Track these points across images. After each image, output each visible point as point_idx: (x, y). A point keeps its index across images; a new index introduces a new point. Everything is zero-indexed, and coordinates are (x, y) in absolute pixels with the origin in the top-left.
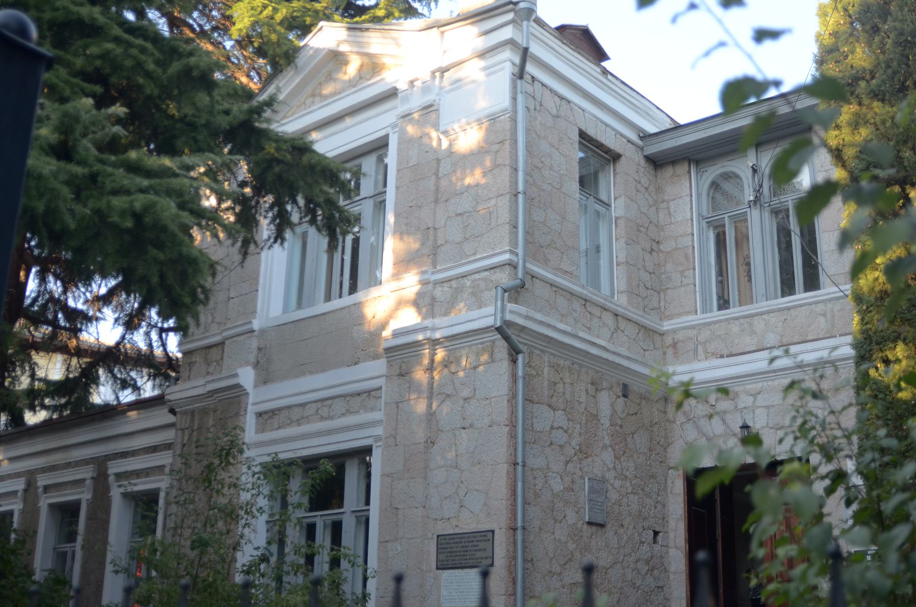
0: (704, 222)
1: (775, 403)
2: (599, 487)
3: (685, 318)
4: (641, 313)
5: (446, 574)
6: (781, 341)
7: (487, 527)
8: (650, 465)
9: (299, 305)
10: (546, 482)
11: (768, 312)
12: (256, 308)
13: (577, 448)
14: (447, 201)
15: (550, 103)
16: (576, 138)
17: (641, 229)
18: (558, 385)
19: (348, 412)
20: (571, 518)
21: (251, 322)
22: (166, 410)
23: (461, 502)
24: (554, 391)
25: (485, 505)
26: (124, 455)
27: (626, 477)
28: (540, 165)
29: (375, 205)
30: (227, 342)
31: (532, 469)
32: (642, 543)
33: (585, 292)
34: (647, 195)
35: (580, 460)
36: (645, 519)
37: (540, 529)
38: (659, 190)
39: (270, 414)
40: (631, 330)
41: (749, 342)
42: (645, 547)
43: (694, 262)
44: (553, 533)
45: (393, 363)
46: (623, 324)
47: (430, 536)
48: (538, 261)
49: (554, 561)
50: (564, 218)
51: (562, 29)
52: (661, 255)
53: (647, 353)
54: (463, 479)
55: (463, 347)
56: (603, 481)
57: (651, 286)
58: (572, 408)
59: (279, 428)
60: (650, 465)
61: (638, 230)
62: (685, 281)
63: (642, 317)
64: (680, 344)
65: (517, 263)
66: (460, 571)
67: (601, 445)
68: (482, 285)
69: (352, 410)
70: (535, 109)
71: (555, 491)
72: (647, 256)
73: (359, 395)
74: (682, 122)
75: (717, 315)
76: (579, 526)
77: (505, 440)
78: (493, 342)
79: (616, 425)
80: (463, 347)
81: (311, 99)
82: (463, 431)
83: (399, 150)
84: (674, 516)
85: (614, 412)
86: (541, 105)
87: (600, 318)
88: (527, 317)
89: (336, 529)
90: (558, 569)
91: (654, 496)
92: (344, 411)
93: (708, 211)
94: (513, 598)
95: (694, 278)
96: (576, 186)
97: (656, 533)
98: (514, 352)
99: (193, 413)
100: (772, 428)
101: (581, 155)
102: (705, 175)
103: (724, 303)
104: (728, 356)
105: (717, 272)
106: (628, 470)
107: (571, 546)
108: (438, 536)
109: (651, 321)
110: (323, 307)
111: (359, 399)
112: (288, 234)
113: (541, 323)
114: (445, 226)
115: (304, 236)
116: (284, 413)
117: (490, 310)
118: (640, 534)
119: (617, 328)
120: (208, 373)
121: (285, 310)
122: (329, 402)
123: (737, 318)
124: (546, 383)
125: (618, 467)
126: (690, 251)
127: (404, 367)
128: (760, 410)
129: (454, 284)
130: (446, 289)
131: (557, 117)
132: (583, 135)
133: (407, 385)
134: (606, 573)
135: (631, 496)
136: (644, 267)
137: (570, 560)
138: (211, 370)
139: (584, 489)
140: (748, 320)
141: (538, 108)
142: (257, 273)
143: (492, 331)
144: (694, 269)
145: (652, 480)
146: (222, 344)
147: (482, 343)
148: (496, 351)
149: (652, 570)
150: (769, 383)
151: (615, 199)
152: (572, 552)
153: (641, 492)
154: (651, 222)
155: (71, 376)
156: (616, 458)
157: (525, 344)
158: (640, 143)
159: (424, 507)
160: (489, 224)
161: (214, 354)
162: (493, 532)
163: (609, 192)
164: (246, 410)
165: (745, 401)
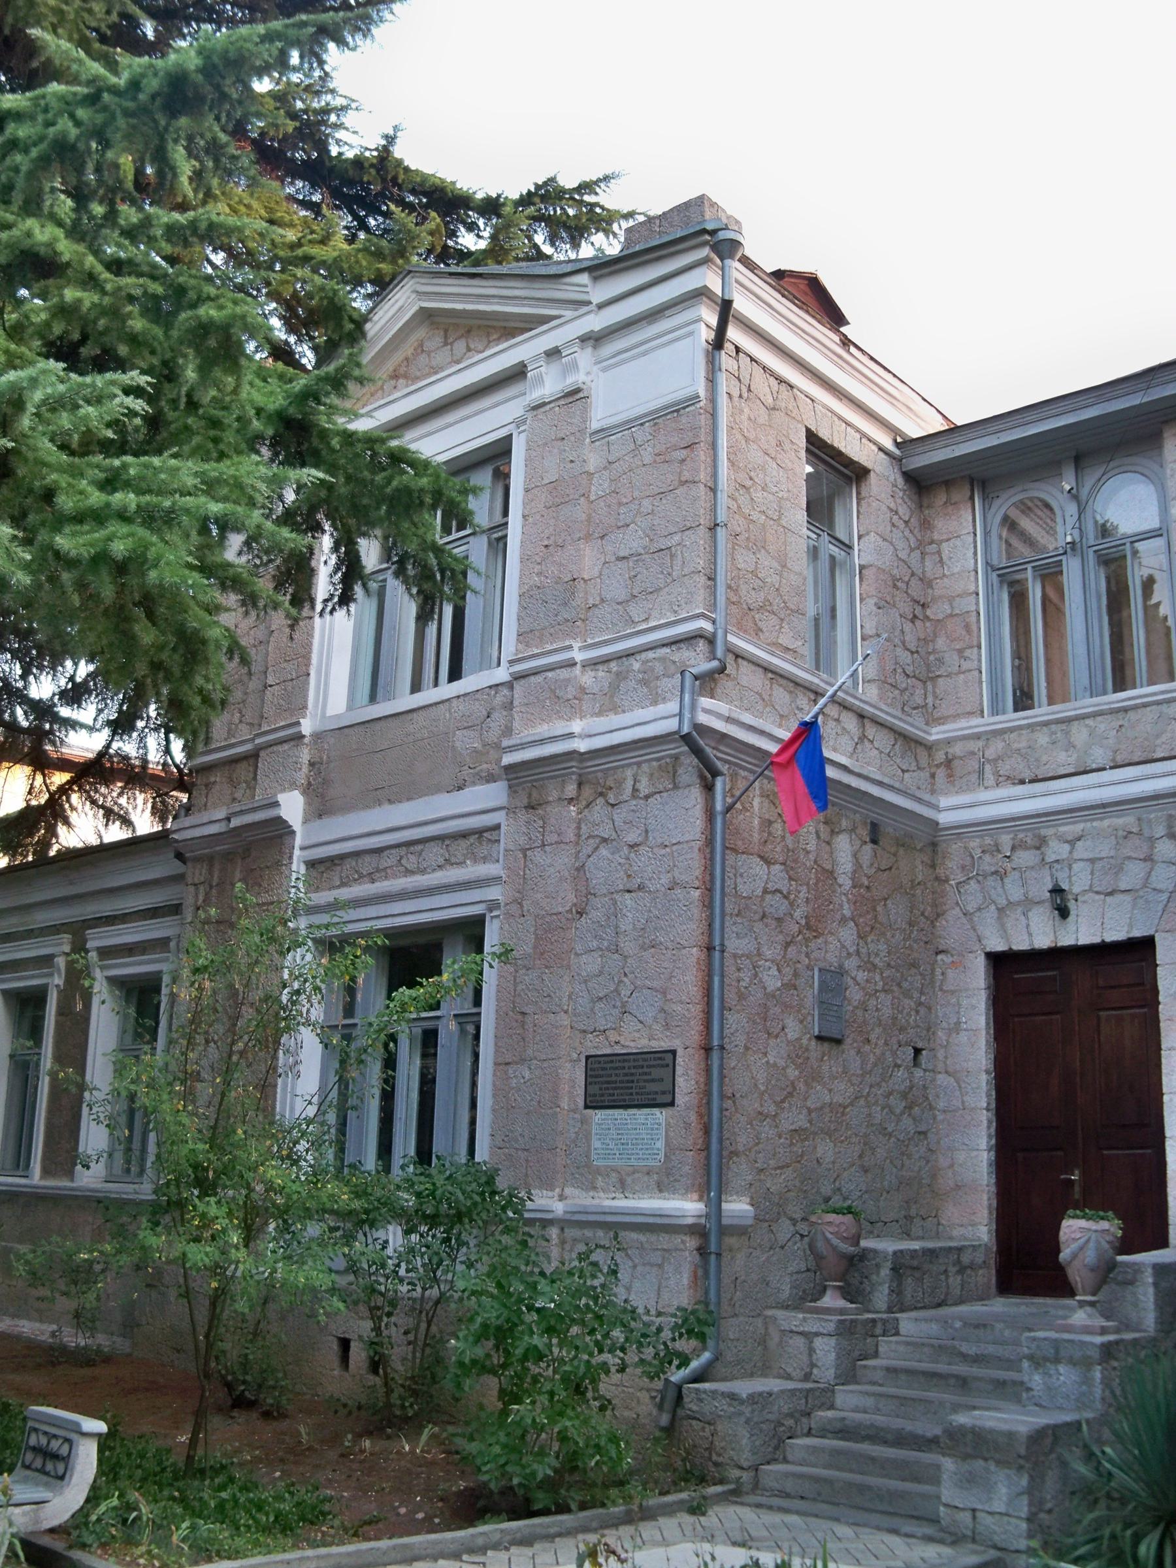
1: (1103, 855)
3: (963, 723)
5: (599, 1115)
23: (624, 1005)
32: (898, 1066)
34: (907, 533)
38: (926, 525)
41: (1063, 760)
47: (575, 1056)
52: (928, 624)
61: (895, 586)
62: (966, 665)
64: (956, 763)
66: (621, 1111)
68: (659, 668)
76: (805, 1042)
82: (627, 895)
84: (944, 1024)
86: (749, 390)
91: (916, 995)
97: (917, 1051)
100: (1098, 893)
107: (793, 1073)
108: (587, 1058)
118: (894, 1053)
125: (863, 951)
128: (1081, 864)
129: (613, 666)
140: (1064, 727)
141: (745, 395)
147: (658, 759)
151: (860, 537)
165: (1056, 850)
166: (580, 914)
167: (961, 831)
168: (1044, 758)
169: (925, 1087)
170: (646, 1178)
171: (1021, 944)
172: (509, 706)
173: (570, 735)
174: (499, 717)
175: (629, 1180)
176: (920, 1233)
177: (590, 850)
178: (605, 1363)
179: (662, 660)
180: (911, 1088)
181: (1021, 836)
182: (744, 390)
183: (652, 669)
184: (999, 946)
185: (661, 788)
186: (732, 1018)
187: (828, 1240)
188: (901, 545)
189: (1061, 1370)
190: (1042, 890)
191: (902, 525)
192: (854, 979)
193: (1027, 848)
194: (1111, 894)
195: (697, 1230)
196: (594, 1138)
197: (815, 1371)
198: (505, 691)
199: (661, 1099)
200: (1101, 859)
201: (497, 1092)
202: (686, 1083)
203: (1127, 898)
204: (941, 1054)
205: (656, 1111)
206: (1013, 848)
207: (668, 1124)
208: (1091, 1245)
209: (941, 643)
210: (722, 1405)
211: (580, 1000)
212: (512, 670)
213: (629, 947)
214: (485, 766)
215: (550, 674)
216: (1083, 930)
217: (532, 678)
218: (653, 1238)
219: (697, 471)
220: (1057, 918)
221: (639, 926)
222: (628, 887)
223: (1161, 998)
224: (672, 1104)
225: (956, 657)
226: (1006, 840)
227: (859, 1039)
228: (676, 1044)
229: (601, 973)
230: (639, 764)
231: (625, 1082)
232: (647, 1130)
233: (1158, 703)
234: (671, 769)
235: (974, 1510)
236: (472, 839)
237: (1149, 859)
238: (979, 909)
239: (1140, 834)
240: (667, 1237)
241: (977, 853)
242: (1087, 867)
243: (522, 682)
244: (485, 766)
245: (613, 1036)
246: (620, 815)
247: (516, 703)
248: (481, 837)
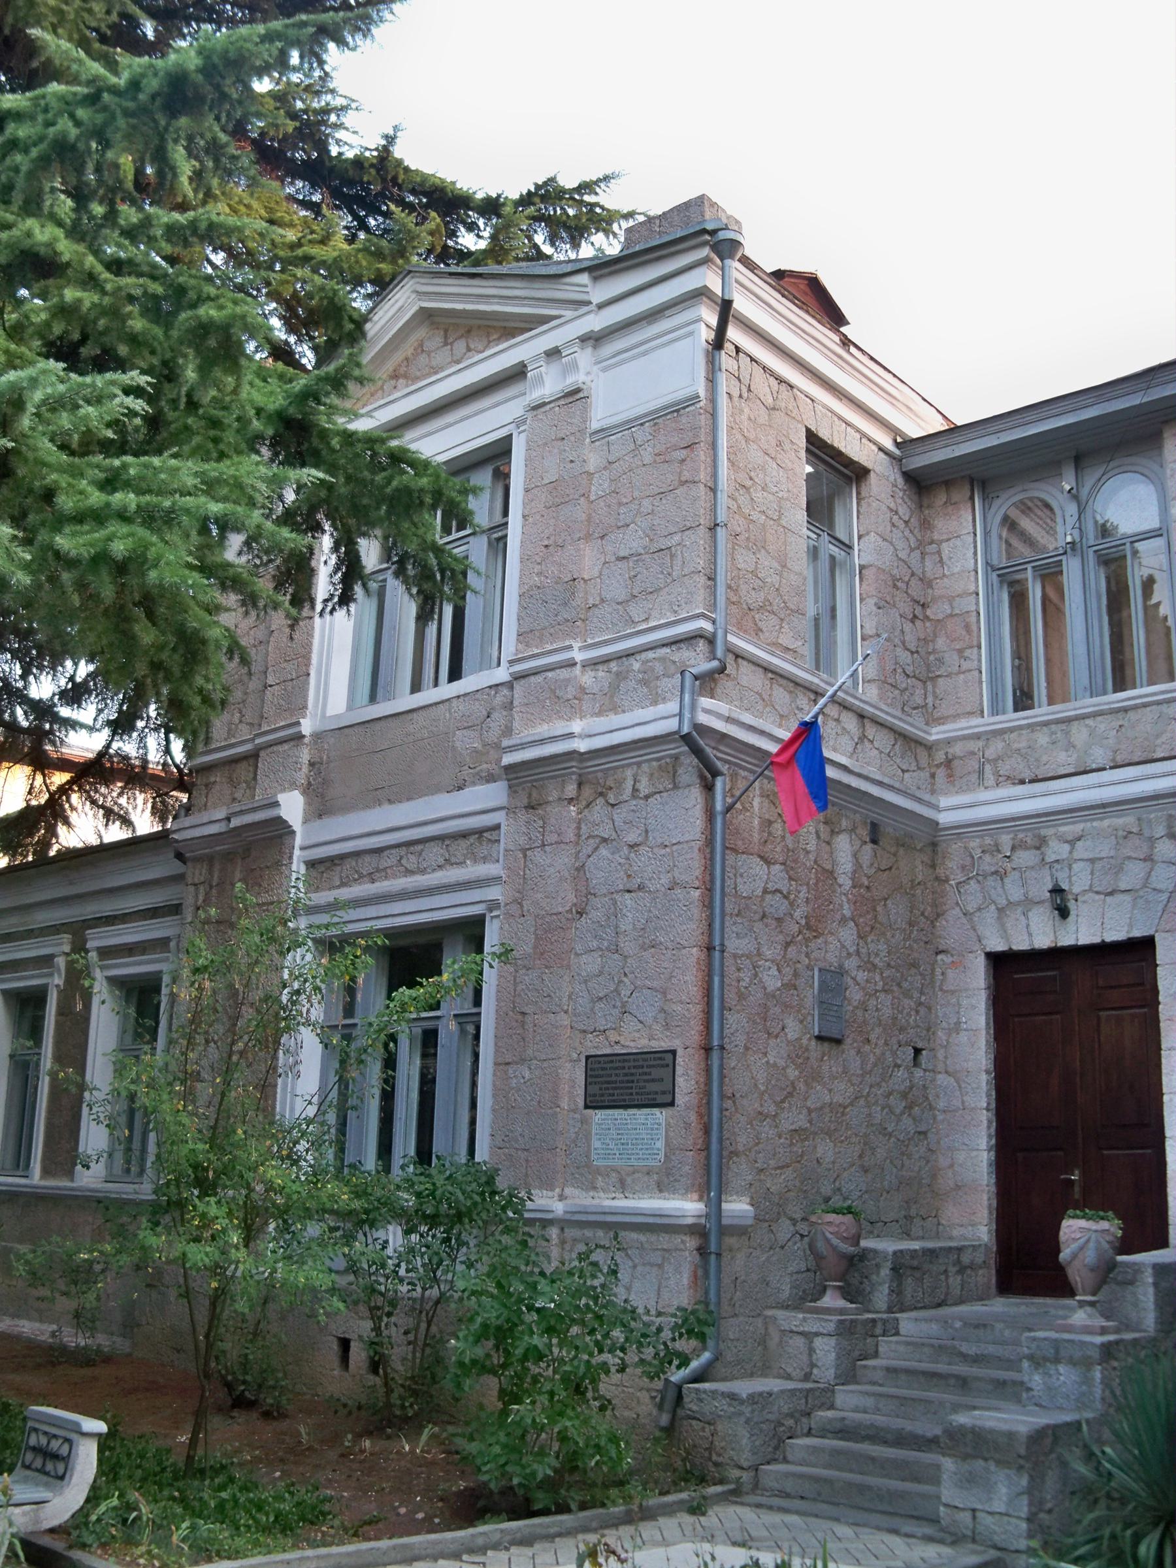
0: (995, 574)
1: (1103, 855)
2: (833, 982)
3: (963, 723)
4: (899, 713)
5: (599, 1115)
6: (1113, 760)
7: (662, 1044)
8: (911, 948)
9: (373, 698)
10: (756, 975)
11: (1094, 715)
12: (306, 701)
13: (803, 922)
14: (602, 538)
15: (763, 386)
16: (802, 443)
17: (899, 584)
18: (775, 825)
20: (793, 1029)
21: (298, 723)
22: (172, 855)
23: (624, 1004)
24: (770, 834)
26: (110, 920)
27: (875, 966)
28: (749, 483)
29: (490, 543)
30: (262, 754)
31: (735, 956)
32: (898, 1066)
33: (816, 680)
34: (907, 533)
35: (807, 940)
36: (902, 1029)
37: (747, 1048)
38: (926, 525)
39: (328, 864)
40: (883, 740)
41: (1063, 760)
42: (901, 1073)
43: (979, 636)
44: (765, 1054)
45: (519, 789)
46: (871, 731)
48: (745, 631)
49: (766, 1097)
50: (784, 566)
51: (779, 275)
52: (928, 624)
53: (907, 775)
55: (629, 765)
56: (841, 972)
57: (918, 671)
58: (795, 861)
59: (343, 884)
60: (911, 948)
61: (895, 586)
62: (966, 665)
63: (900, 719)
64: (956, 763)
65: (714, 635)
66: (621, 1111)
67: (838, 917)
68: (659, 668)
69: (453, 860)
72: (908, 627)
74: (961, 419)
75: (1012, 718)
76: (804, 1041)
77: (696, 912)
78: (676, 758)
79: (861, 886)
80: (629, 765)
81: (393, 382)
82: (627, 895)
83: (528, 461)
84: (944, 1024)
85: (858, 866)
86: (749, 390)
87: (837, 720)
88: (729, 720)
89: (429, 1039)
90: (772, 1109)
91: (916, 995)
92: (441, 861)
93: (1000, 557)
94: (704, 1154)
95: (980, 661)
96: (802, 516)
97: (917, 1051)
98: (708, 776)
99: (210, 859)
100: (1097, 893)
101: (809, 469)
102: (997, 503)
103: (1024, 699)
104: (1031, 782)
105: (1013, 652)
106: (877, 955)
107: (793, 1073)
108: (587, 1058)
109: (912, 725)
110: (406, 701)
112: (358, 589)
113: (751, 728)
115: (381, 595)
116: (350, 863)
117: (672, 706)
118: (894, 1053)
119: (863, 738)
120: (234, 799)
121: (350, 707)
122: (419, 847)
123: (1046, 724)
125: (864, 951)
126: (973, 619)
127: (535, 794)
128: (1081, 864)
129: (613, 666)
130: (601, 674)
131: (774, 409)
132: (813, 439)
134: (843, 1114)
135: (882, 996)
136: (903, 643)
137: (790, 1094)
138: (238, 795)
139: (812, 986)
140: (1064, 726)
141: (745, 395)
142: (308, 646)
143: (674, 741)
144: (979, 647)
145: (913, 971)
146: (253, 757)
147: (658, 759)
148: (680, 771)
149: (909, 1107)
150: (1095, 824)
151: (860, 537)
152: (793, 1083)
153: (895, 988)
154: (913, 574)
155: (34, 803)
156: (860, 937)
157: (726, 761)
158: (897, 452)
161: (243, 770)
162: (674, 1052)
163: (850, 526)
164: (291, 858)
165: (1056, 850)
166: (580, 914)
167: (961, 830)
168: (1045, 758)
170: (646, 1178)
171: (1021, 944)
172: (509, 706)
173: (570, 736)
175: (629, 1180)
177: (590, 850)
179: (662, 660)
180: (911, 1088)
181: (1021, 836)
182: (744, 390)
184: (999, 946)
187: (828, 1240)
188: (901, 545)
189: (1061, 1370)
190: (1042, 890)
191: (902, 525)
192: (854, 979)
193: (1027, 848)
194: (1111, 894)
195: (698, 1230)
196: (594, 1138)
197: (815, 1371)
198: (505, 691)
199: (660, 1099)
201: (497, 1092)
202: (686, 1083)
203: (1127, 898)
204: (941, 1054)
205: (656, 1111)
206: (1013, 848)
207: (668, 1124)
208: (1092, 1245)
210: (722, 1405)
211: (580, 1000)
212: (512, 670)
213: (628, 947)
214: (485, 766)
215: (550, 674)
216: (1083, 930)
217: (532, 679)
218: (653, 1238)
219: (697, 471)
220: (1057, 918)
221: (639, 926)
222: (628, 887)
223: (1161, 998)
224: (672, 1104)
225: (956, 657)
226: (1006, 840)
228: (676, 1044)
229: (601, 973)
230: (639, 764)
231: (625, 1082)
232: (647, 1130)
233: (1158, 703)
234: (671, 769)
235: (974, 1510)
237: (1149, 859)
238: (979, 909)
239: (1140, 834)
240: (667, 1237)
241: (977, 853)
242: (1087, 867)
243: (523, 682)
244: (485, 766)
245: (613, 1036)
246: (620, 815)
247: (516, 703)
248: (481, 837)
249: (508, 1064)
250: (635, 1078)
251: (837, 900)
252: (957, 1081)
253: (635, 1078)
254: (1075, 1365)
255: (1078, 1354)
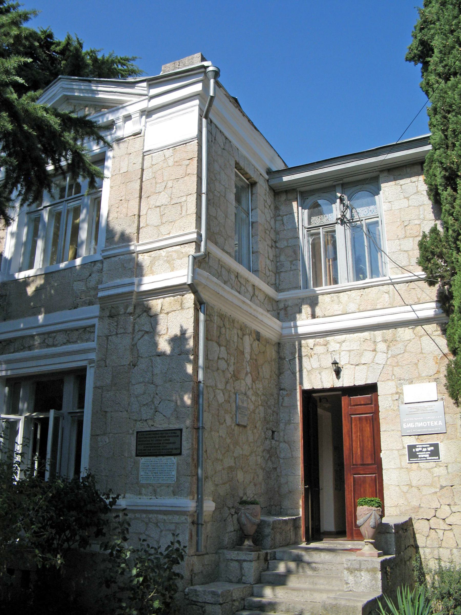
1: (355, 348)
5: (143, 460)
7: (177, 426)
19: (68, 342)
23: (156, 408)
25: (175, 410)
32: (266, 439)
34: (270, 211)
38: (277, 208)
47: (131, 432)
52: (277, 250)
54: (157, 392)
61: (265, 232)
62: (293, 267)
64: (289, 308)
68: (175, 256)
70: (212, 141)
71: (220, 403)
73: (77, 330)
76: (233, 427)
82: (158, 358)
84: (283, 421)
86: (215, 140)
91: (272, 407)
92: (65, 341)
97: (273, 432)
100: (352, 364)
102: (307, 201)
107: (228, 441)
108: (137, 432)
111: (77, 333)
114: (146, 214)
118: (265, 433)
124: (215, 326)
125: (254, 387)
128: (344, 352)
133: (116, 324)
141: (214, 141)
151: (252, 210)
158: (267, 177)
159: (127, 411)
160: (181, 214)
166: (134, 366)
169: (276, 448)
172: (101, 271)
174: (95, 276)
175: (158, 490)
176: (274, 513)
177: (140, 336)
178: (196, 591)
180: (271, 448)
182: (213, 139)
183: (171, 256)
185: (175, 309)
186: (205, 414)
187: (247, 517)
189: (363, 574)
191: (268, 207)
192: (251, 400)
193: (320, 345)
194: (357, 365)
196: (140, 470)
197: (243, 578)
198: (99, 265)
199: (174, 452)
200: (353, 350)
201: (92, 448)
202: (187, 445)
203: (365, 366)
205: (172, 457)
206: (314, 345)
208: (373, 516)
209: (282, 258)
210: (209, 598)
212: (103, 254)
213: (158, 380)
214: (88, 298)
215: (121, 257)
216: (346, 381)
217: (113, 259)
218: (170, 517)
221: (164, 371)
223: (380, 410)
224: (180, 454)
225: (289, 263)
227: (252, 426)
229: (144, 393)
233: (378, 286)
236: (81, 331)
237: (374, 350)
243: (108, 260)
244: (88, 298)
245: (151, 423)
247: (104, 269)
248: (87, 330)
249: (97, 435)
250: (161, 442)
251: (244, 364)
252: (289, 446)
253: (161, 442)
254: (369, 571)
255: (370, 567)
